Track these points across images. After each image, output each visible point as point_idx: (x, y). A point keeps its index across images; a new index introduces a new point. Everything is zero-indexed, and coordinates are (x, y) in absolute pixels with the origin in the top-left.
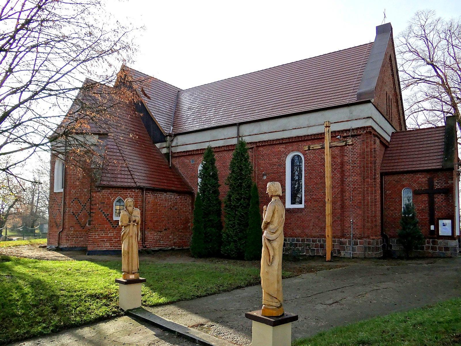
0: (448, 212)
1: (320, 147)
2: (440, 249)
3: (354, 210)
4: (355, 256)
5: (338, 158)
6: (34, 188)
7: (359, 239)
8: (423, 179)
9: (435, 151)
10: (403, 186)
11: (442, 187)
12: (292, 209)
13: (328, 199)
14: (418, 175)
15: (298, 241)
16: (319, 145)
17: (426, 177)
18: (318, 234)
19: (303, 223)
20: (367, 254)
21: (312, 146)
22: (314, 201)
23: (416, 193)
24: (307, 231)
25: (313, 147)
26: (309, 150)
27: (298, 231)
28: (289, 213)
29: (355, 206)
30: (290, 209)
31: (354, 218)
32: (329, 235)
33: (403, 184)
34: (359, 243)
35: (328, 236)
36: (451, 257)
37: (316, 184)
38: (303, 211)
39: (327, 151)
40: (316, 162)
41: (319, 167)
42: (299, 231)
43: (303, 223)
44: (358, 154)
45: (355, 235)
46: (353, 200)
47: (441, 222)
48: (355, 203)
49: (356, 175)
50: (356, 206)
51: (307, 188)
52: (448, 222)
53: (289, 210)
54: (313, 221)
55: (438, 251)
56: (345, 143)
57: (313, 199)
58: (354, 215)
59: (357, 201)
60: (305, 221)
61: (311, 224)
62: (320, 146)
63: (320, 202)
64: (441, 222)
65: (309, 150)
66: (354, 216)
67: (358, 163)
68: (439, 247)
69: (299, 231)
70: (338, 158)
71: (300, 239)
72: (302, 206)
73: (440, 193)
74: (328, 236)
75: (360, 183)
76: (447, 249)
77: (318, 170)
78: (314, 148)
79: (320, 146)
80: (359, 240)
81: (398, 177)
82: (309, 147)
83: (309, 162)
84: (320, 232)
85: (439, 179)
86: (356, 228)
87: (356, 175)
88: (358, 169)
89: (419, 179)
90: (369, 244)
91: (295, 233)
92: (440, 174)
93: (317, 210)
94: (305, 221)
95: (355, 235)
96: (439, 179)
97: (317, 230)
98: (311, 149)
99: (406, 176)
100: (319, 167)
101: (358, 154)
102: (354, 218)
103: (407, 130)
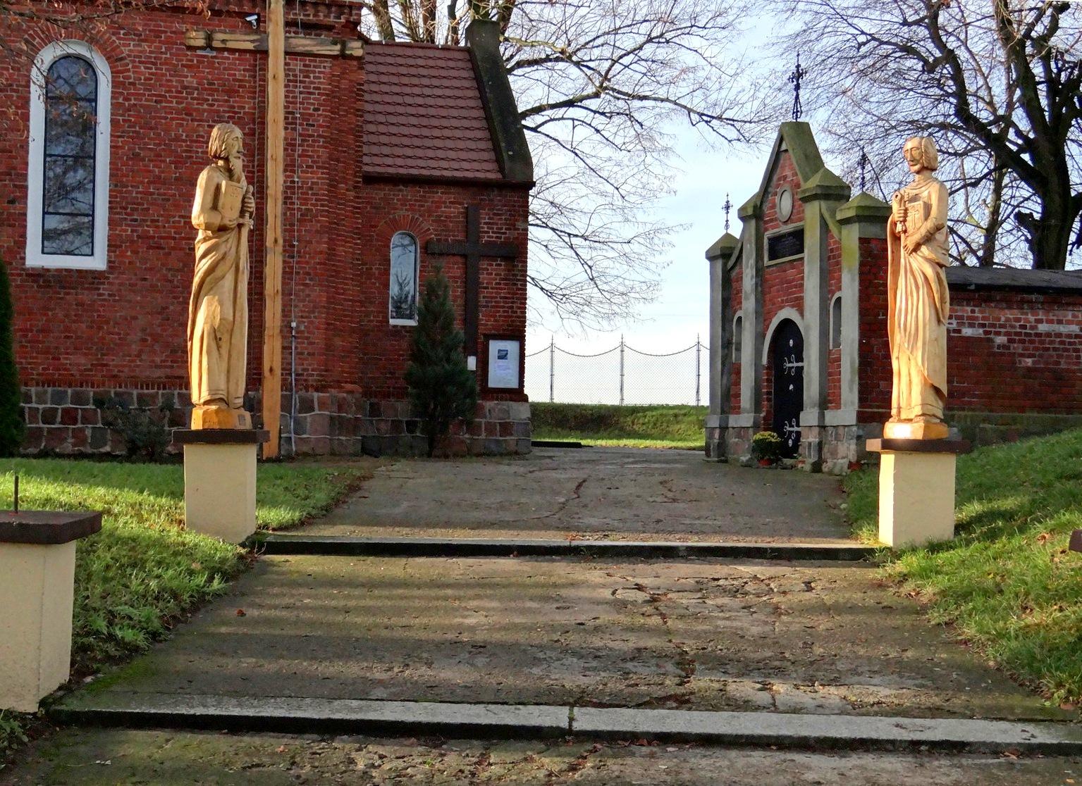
0: (512, 317)
1: (250, 46)
2: (490, 429)
3: (303, 291)
4: (305, 449)
5: (243, 97)
6: (871, 100)
7: (317, 390)
8: (451, 207)
9: (402, 120)
10: (395, 226)
11: (500, 238)
12: (57, 270)
13: (276, 241)
14: (439, 194)
15: (78, 399)
16: (247, 38)
17: (460, 204)
18: (158, 373)
19: (100, 328)
20: (336, 442)
21: (219, 36)
22: (150, 248)
23: (428, 251)
24: (114, 361)
25: (224, 41)
26: (209, 46)
27: (77, 362)
28: (39, 286)
29: (304, 274)
30: (48, 270)
31: (302, 317)
32: (275, 367)
33: (394, 217)
34: (316, 406)
35: (271, 370)
36: (516, 453)
37: (157, 180)
38: (103, 283)
39: (276, 64)
40: (160, 99)
41: (172, 119)
42: (83, 361)
43: (100, 328)
44: (323, 94)
45: (302, 375)
46: (299, 252)
47: (495, 346)
48: (307, 263)
49: (312, 167)
50: (308, 274)
51: (121, 192)
52: (511, 346)
53: (39, 275)
54: (142, 321)
55: (483, 436)
56: (338, 47)
57: (145, 237)
58: (301, 304)
59: (313, 258)
60: (107, 323)
61: (136, 336)
62: (252, 41)
63: (173, 253)
64: (495, 346)
65: (209, 46)
66: (302, 311)
67: (321, 126)
68: (488, 424)
69: (83, 361)
70: (243, 97)
71: (91, 392)
72: (98, 262)
73: (494, 258)
74: (271, 370)
75: (324, 195)
76: (506, 428)
77: (167, 131)
78: (230, 45)
79: (252, 41)
80: (316, 395)
81: (382, 194)
82: (209, 38)
83: (133, 94)
84: (166, 367)
85: (494, 214)
86: (309, 354)
87: (312, 167)
88: (318, 146)
89: (438, 207)
90: (340, 409)
91: (65, 369)
92: (495, 196)
93: (158, 280)
94: (107, 323)
95: (302, 375)
96: (494, 214)
97: (158, 360)
98: (216, 44)
99: (407, 193)
100: (172, 119)
101: (323, 94)
102: (302, 317)
103: (397, 40)
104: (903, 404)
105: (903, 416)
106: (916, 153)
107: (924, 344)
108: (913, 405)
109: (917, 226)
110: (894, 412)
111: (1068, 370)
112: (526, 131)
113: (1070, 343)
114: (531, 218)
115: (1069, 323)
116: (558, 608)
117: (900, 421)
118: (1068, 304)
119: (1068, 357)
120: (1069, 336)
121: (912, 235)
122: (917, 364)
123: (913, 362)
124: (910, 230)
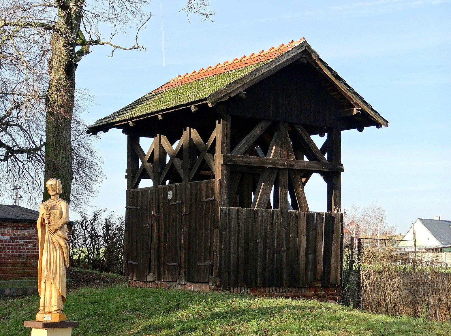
104: (47, 304)
105: (46, 310)
106: (54, 187)
107: (60, 277)
108: (52, 305)
109: (56, 221)
110: (41, 308)
111: (4, 259)
112: (45, 151)
113: (6, 245)
114: (14, 204)
115: (6, 235)
116: (270, 277)
117: (45, 313)
118: (6, 226)
119: (5, 252)
120: (6, 242)
121: (53, 225)
122: (56, 286)
123: (53, 285)
124: (52, 223)
